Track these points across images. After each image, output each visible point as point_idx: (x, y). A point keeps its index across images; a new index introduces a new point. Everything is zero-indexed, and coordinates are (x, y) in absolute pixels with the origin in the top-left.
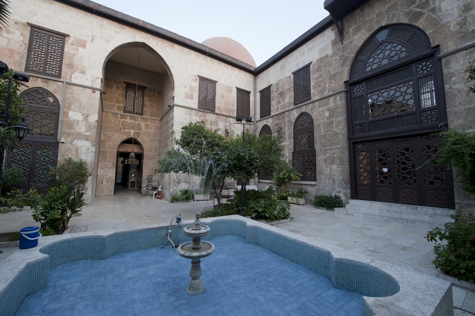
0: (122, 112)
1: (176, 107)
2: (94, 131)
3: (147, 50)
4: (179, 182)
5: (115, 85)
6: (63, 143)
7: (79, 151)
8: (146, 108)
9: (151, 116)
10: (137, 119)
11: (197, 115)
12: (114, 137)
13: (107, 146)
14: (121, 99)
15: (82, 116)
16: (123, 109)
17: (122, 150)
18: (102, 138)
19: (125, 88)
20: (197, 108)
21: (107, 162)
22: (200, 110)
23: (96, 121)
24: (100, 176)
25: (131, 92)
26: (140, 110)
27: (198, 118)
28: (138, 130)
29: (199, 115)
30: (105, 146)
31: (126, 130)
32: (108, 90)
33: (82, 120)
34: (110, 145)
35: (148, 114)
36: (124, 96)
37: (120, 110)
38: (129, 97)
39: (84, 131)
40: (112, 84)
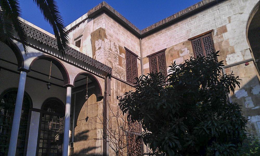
33: (247, 95)
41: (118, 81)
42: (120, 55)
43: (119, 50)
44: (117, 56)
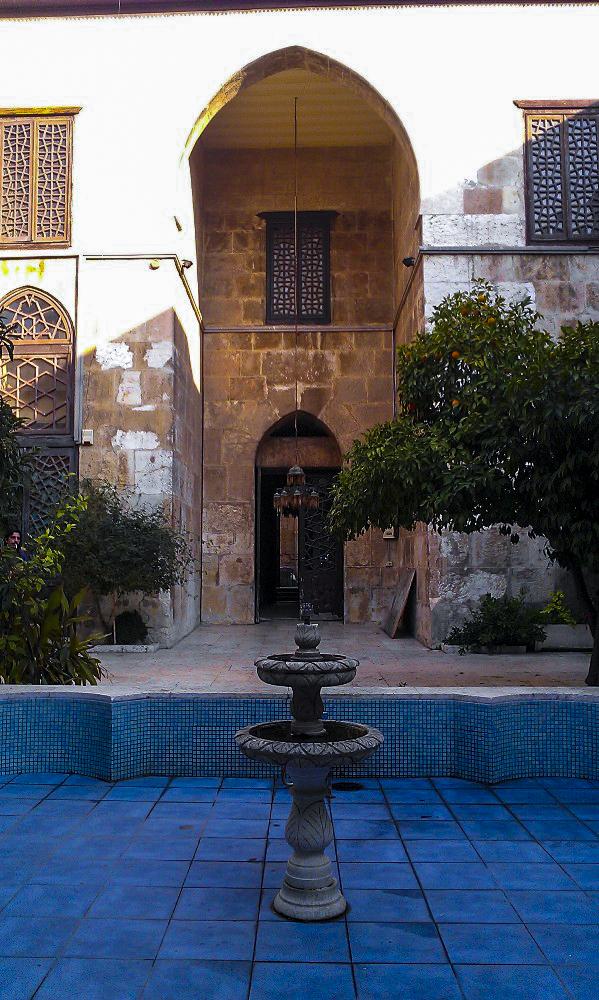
0: (259, 325)
1: (435, 259)
2: (165, 397)
3: (313, 68)
4: (463, 570)
5: (233, 232)
6: (87, 444)
7: (130, 464)
8: (338, 293)
9: (359, 320)
10: (311, 340)
11: (523, 275)
12: (242, 417)
13: (224, 450)
14: (256, 277)
15: (130, 353)
16: (262, 313)
17: (271, 461)
18: (206, 426)
19: (264, 235)
20: (521, 244)
21: (228, 507)
22: (543, 247)
23: (169, 362)
24: (210, 554)
25: (284, 243)
26: (319, 304)
27: (530, 285)
28: (318, 379)
29: (533, 274)
30: (219, 451)
31: (278, 388)
32: (213, 257)
33: (130, 366)
34: (230, 447)
35: (349, 315)
36: (264, 265)
37: (255, 317)
38: (278, 266)
39: (139, 401)
40: (224, 231)
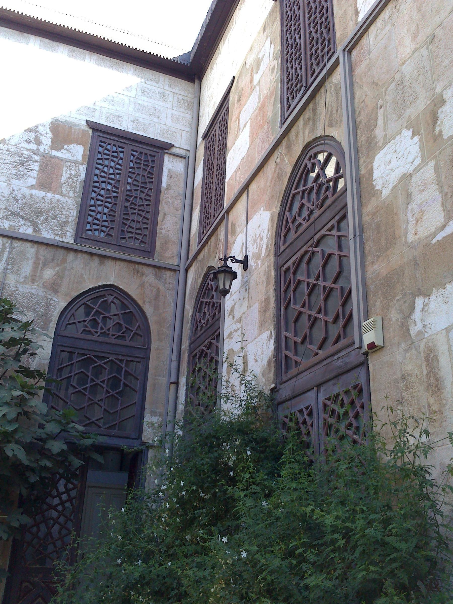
41: (17, 244)
42: (54, 153)
43: (50, 135)
44: (36, 158)
